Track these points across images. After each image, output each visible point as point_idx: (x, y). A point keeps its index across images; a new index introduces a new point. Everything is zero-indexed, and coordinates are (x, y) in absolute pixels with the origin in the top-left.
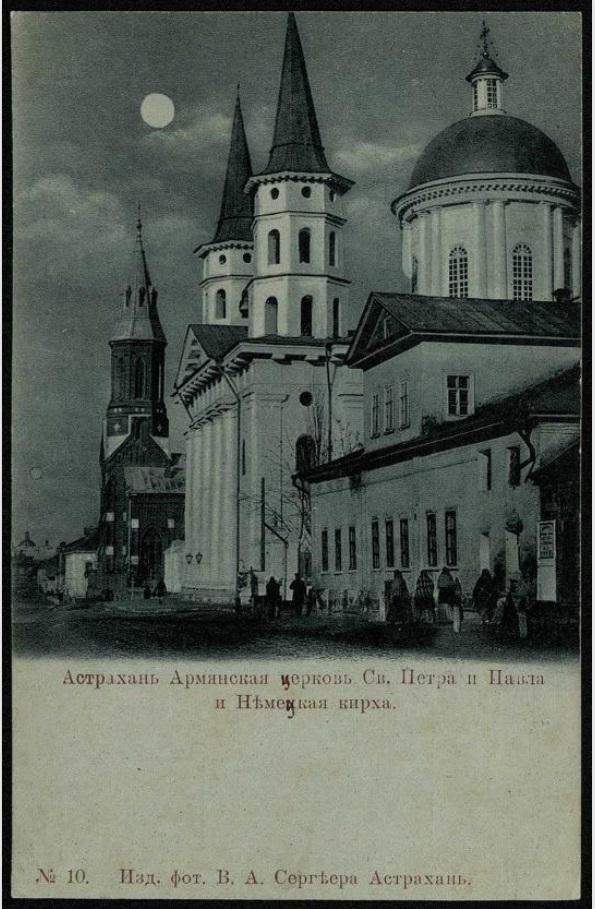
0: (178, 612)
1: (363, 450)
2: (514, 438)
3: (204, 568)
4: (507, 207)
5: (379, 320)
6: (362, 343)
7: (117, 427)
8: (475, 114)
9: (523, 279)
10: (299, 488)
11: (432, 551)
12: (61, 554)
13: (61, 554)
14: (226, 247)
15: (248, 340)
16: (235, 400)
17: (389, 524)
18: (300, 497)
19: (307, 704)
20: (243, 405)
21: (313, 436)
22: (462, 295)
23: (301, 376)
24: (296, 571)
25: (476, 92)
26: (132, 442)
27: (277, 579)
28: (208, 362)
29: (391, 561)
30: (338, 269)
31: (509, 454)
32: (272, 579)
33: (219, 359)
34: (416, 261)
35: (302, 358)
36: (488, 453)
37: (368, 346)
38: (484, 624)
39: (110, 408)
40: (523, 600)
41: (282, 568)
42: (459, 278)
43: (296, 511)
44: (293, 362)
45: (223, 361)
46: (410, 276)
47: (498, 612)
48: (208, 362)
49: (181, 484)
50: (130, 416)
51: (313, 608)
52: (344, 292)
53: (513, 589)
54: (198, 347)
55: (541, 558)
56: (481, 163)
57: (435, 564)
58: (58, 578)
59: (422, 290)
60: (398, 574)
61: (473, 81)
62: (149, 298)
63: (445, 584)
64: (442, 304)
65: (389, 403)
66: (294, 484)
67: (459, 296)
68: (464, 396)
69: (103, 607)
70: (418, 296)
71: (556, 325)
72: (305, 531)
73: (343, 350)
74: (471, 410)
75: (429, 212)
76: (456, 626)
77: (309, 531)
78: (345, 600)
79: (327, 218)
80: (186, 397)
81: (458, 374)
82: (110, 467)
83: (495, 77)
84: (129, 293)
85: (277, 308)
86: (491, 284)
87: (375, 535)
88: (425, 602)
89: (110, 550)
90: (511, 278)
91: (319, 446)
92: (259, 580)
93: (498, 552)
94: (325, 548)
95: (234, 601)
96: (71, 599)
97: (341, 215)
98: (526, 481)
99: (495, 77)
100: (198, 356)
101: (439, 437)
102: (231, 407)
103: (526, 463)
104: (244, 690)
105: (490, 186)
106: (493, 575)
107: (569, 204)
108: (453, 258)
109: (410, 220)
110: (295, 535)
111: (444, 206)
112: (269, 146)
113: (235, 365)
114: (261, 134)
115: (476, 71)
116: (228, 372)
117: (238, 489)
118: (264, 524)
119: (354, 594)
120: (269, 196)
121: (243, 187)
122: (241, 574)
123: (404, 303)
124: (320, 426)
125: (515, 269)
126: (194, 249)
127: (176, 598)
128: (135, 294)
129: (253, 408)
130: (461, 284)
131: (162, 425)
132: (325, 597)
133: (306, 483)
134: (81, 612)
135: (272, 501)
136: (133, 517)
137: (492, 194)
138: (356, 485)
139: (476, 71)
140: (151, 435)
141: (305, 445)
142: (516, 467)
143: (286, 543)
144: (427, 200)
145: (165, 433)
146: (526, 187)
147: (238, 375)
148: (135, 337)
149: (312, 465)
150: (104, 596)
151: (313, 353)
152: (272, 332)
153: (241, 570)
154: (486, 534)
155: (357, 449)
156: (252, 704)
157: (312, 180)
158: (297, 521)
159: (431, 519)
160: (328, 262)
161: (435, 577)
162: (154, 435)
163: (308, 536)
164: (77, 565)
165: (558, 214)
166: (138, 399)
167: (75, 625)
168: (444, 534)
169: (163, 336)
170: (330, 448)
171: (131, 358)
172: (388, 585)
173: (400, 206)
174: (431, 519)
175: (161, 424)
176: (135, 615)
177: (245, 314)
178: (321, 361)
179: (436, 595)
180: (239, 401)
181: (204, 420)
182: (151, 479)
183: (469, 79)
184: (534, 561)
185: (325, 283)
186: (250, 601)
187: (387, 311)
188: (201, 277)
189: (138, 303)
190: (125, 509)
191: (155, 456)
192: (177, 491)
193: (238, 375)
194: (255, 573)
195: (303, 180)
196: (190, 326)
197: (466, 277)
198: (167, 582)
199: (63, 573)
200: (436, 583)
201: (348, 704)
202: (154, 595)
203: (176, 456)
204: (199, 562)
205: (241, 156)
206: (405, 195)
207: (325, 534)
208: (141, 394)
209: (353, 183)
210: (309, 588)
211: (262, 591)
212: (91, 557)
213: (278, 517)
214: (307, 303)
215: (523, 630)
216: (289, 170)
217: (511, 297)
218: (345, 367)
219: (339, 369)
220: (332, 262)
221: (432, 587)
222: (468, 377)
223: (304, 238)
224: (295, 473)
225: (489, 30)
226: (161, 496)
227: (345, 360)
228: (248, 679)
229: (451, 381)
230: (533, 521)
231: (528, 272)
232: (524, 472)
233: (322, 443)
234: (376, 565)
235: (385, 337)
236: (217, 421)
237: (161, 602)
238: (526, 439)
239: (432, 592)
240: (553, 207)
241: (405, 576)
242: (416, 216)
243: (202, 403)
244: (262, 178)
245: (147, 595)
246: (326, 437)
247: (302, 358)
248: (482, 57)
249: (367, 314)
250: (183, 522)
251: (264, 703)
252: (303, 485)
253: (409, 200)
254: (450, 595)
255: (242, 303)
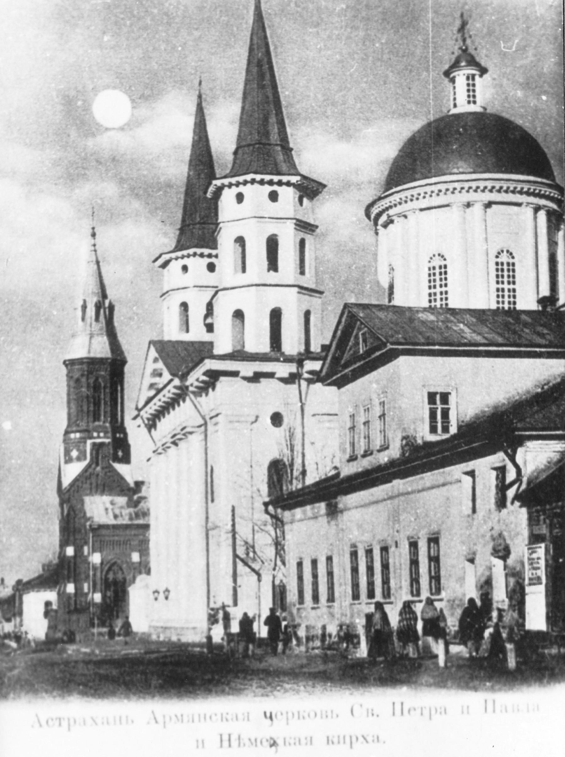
0: (146, 653)
1: (338, 475)
2: (498, 459)
3: (170, 604)
4: (488, 210)
5: (354, 334)
6: (336, 360)
7: (74, 454)
8: (454, 111)
9: (506, 286)
10: (272, 516)
11: (415, 580)
12: (17, 594)
13: (17, 594)
14: (188, 256)
15: (213, 357)
16: (202, 422)
17: (369, 552)
18: (272, 525)
19: (292, 742)
20: (210, 428)
21: (285, 460)
22: (441, 305)
23: (275, 395)
24: (271, 606)
25: (454, 88)
26: (90, 470)
27: (251, 615)
28: (171, 380)
29: (371, 594)
30: (308, 281)
31: (494, 473)
32: (245, 614)
33: (184, 377)
34: (393, 269)
35: (271, 375)
36: (472, 474)
37: (343, 362)
38: (471, 656)
39: (67, 433)
40: (511, 630)
41: (255, 602)
42: (438, 286)
43: (269, 541)
44: (262, 380)
45: (186, 380)
46: (386, 286)
47: (485, 644)
48: (171, 380)
49: (146, 514)
50: (89, 442)
51: (289, 645)
52: (315, 303)
53: (500, 617)
54: (160, 365)
55: (530, 584)
56: (460, 163)
57: (418, 594)
58: (15, 619)
59: (399, 300)
60: (379, 606)
61: (452, 76)
62: (105, 312)
63: (430, 615)
64: (420, 315)
65: (366, 423)
66: (267, 512)
67: (439, 306)
68: (445, 414)
69: (64, 650)
70: (394, 307)
71: (542, 336)
72: (279, 563)
73: (316, 365)
74: (453, 430)
75: (406, 217)
76: (441, 661)
77: (284, 563)
78: (324, 635)
79: (296, 224)
80: (148, 419)
81: (439, 391)
82: (70, 499)
83: (474, 72)
84: (84, 307)
85: (243, 322)
86: (474, 292)
87: (355, 565)
88: (407, 634)
89: (70, 588)
90: (494, 286)
91: (292, 470)
92: (231, 616)
93: (483, 579)
94: (300, 578)
95: (205, 640)
96: (29, 642)
97: (312, 222)
98: (512, 503)
99: (474, 72)
100: (160, 375)
101: (419, 459)
102: (197, 429)
103: (512, 484)
104: (226, 728)
105: (462, 188)
106: (479, 603)
107: (554, 206)
108: (431, 265)
109: (385, 226)
110: (269, 566)
111: (421, 210)
112: (234, 147)
113: (201, 385)
114: (224, 137)
115: (455, 65)
116: (193, 393)
117: (207, 518)
118: (235, 556)
119: (332, 629)
120: (234, 200)
121: (205, 192)
122: (212, 609)
123: (381, 315)
124: (292, 450)
125: (497, 276)
126: (153, 258)
127: (145, 640)
128: (91, 311)
129: (219, 434)
130: (441, 293)
131: (123, 451)
132: (302, 633)
133: (279, 511)
134: (43, 655)
135: (244, 531)
136: (94, 551)
137: (472, 196)
138: (333, 512)
139: (455, 65)
140: (111, 462)
141: (277, 470)
142: (502, 488)
143: (259, 575)
144: (409, 202)
145: (126, 459)
146: (508, 188)
147: (204, 395)
148: (92, 355)
149: (286, 491)
150: (65, 638)
151: (283, 370)
152: (239, 348)
153: (212, 605)
154: (472, 561)
155: (333, 472)
156: (234, 743)
157: (280, 183)
158: (270, 552)
159: (414, 545)
160: (299, 271)
161: (418, 608)
162: (114, 461)
163: (282, 567)
164: (35, 604)
165: (542, 216)
166: (97, 423)
167: (34, 667)
168: (426, 561)
169: (122, 353)
170: (304, 473)
171: (88, 379)
172: (369, 617)
173: (375, 211)
174: (414, 545)
175: (121, 448)
176: (99, 658)
177: (210, 328)
178: (292, 379)
179: (420, 626)
180: (206, 424)
181: (168, 445)
182: (113, 509)
183: (447, 74)
184: (522, 589)
185: (296, 295)
186: (223, 639)
187: (362, 323)
188: (162, 288)
189: (94, 317)
190: (86, 543)
191: (114, 485)
192: (141, 522)
193: (204, 395)
194: (228, 609)
195: (271, 183)
196: (150, 343)
197: (446, 285)
198: (132, 620)
199: (20, 613)
200: (419, 615)
201: (336, 740)
202: (119, 635)
203: (139, 484)
204: (167, 598)
205: (202, 157)
206: (380, 199)
207: (300, 565)
208: (99, 415)
209: (324, 186)
210: (284, 623)
211: (235, 628)
212: (51, 596)
213: (250, 547)
214: (276, 316)
215: (512, 662)
216: (256, 173)
217: (494, 306)
218: (319, 385)
219: (312, 386)
220: (302, 273)
221: (416, 619)
222: (450, 393)
223: (272, 245)
224: (267, 499)
225: (467, 23)
226: (127, 527)
227: (317, 377)
228: (229, 717)
229: (432, 397)
230: (519, 548)
231: (511, 279)
232: (511, 493)
233: (295, 468)
234: (356, 596)
235: (361, 352)
236: (182, 444)
237: (126, 643)
238: (512, 459)
239: (416, 624)
240: (537, 209)
241: (387, 608)
242: (392, 222)
243: (168, 425)
244: (226, 181)
245: (112, 634)
246: (298, 461)
247: (271, 375)
248: (460, 52)
249: (340, 327)
250: (148, 554)
251: (247, 742)
252: (276, 512)
253: (385, 203)
254: (435, 627)
255: (206, 317)
